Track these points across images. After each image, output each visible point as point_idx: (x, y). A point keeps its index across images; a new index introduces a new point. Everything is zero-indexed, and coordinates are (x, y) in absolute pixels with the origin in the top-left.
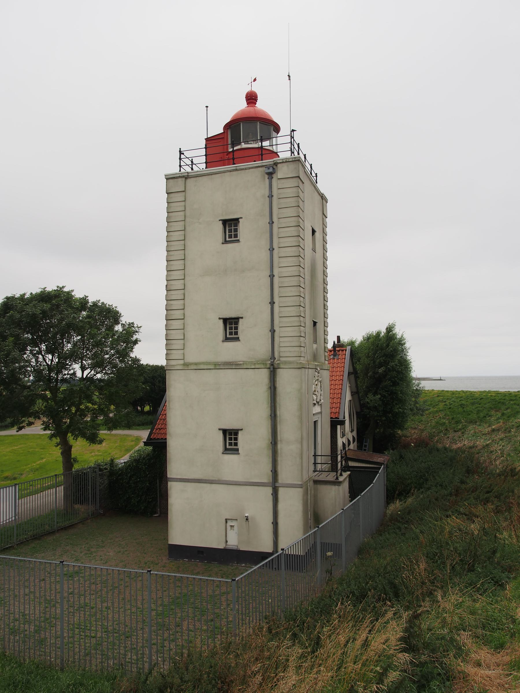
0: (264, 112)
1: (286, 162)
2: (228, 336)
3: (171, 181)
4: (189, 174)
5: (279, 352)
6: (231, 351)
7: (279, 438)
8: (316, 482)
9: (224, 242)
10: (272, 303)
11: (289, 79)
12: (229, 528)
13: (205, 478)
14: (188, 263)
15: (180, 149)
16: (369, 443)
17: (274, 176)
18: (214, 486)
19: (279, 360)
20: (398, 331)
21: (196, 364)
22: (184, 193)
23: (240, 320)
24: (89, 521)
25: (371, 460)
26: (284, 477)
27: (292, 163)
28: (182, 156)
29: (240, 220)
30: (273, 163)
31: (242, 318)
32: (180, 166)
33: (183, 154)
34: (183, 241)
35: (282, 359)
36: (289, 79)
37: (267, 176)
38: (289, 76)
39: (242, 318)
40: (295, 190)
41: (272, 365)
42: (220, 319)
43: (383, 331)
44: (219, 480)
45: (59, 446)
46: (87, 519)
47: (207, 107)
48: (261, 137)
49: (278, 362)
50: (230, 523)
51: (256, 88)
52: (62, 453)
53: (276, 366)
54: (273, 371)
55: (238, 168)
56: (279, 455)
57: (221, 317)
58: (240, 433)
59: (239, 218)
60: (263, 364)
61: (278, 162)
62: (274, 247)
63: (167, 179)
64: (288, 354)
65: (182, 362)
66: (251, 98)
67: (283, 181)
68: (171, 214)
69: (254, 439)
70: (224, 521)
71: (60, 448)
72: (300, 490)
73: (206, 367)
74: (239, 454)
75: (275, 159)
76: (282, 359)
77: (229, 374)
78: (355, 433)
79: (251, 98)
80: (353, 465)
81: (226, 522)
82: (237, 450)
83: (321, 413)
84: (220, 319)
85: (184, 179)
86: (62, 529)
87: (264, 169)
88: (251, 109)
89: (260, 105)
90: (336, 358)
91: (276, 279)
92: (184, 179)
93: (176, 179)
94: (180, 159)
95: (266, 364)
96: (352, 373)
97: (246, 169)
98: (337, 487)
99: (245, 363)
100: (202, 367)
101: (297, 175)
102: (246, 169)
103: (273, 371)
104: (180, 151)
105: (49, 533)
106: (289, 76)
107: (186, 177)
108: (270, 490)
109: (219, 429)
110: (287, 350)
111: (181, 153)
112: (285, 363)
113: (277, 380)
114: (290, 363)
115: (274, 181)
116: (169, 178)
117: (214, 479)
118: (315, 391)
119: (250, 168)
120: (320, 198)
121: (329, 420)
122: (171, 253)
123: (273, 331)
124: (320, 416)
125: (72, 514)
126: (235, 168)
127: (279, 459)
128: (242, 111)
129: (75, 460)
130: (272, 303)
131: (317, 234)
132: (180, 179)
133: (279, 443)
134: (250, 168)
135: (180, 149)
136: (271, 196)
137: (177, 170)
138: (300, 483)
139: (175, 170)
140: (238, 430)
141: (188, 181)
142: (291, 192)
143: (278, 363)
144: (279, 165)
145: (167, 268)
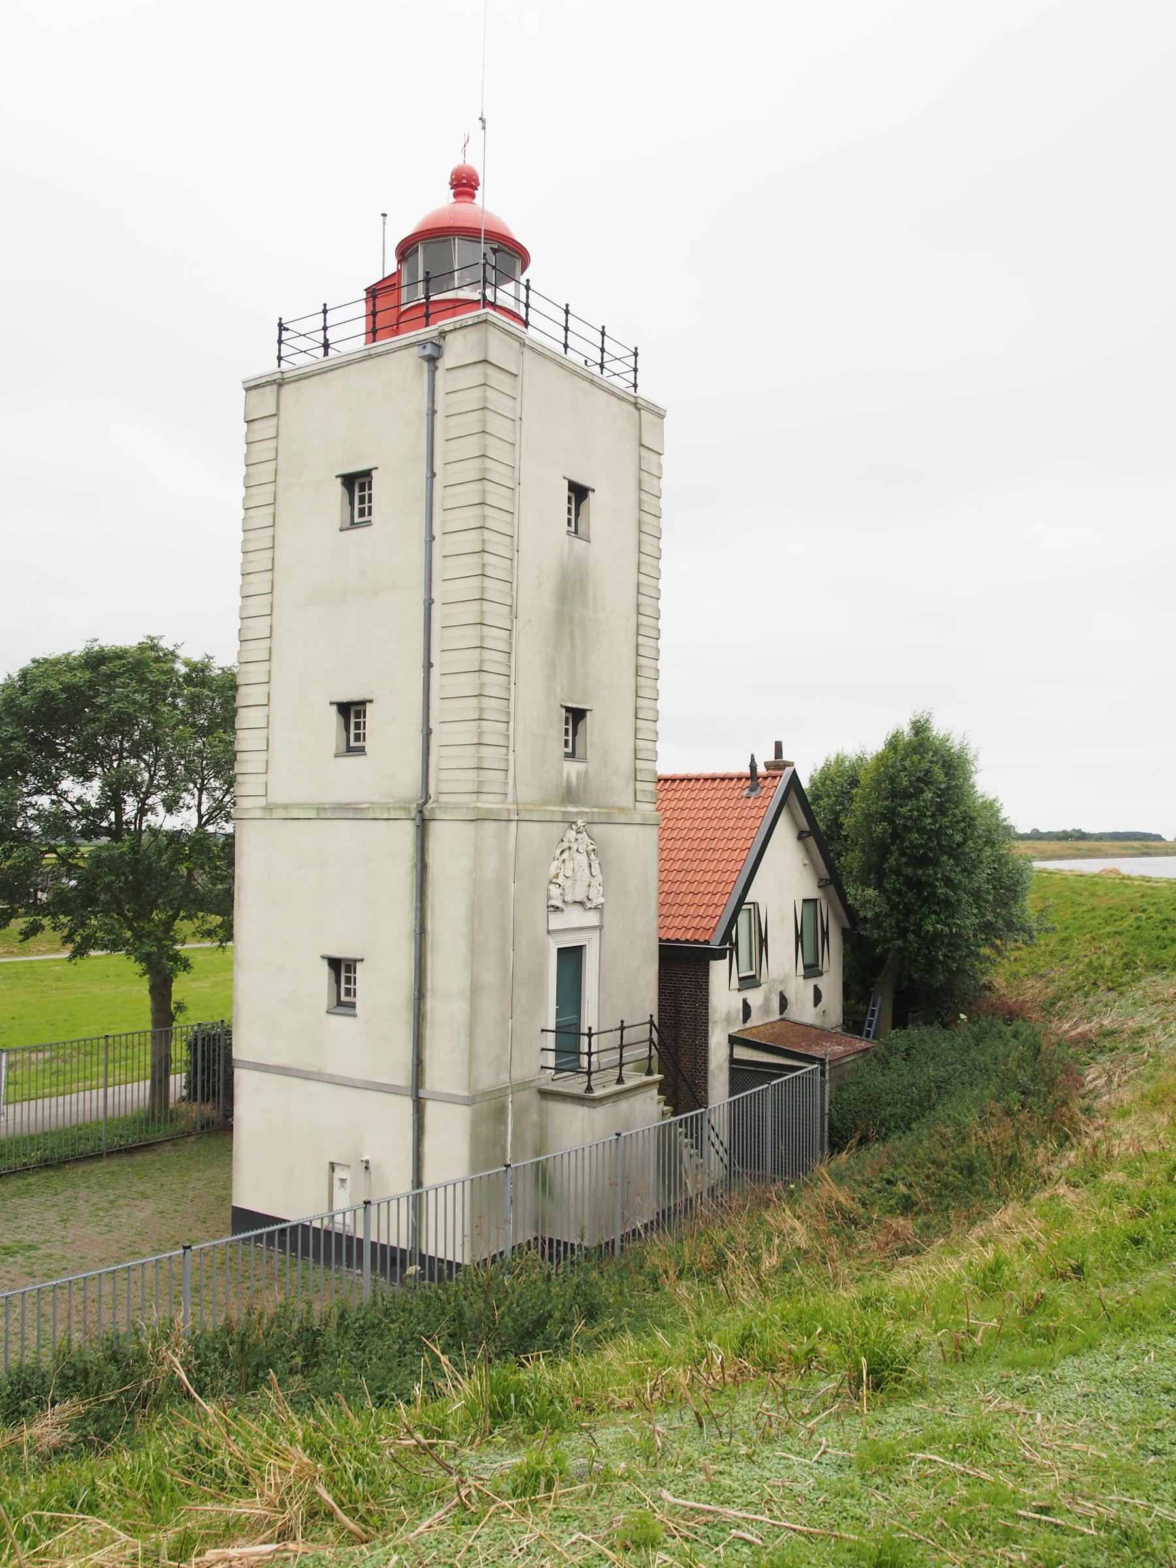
1: (461, 328)
2: (352, 744)
3: (253, 393)
4: (285, 376)
5: (438, 781)
6: (355, 779)
7: (429, 986)
8: (544, 1094)
9: (348, 525)
10: (428, 666)
11: (484, 128)
12: (337, 1183)
13: (299, 1067)
14: (279, 577)
16: (881, 1006)
17: (440, 363)
18: (312, 1085)
19: (436, 801)
20: (939, 728)
21: (286, 807)
22: (275, 419)
23: (368, 705)
24: (193, 1139)
25: (810, 1053)
26: (438, 1078)
27: (470, 329)
28: (285, 335)
29: (374, 473)
30: (436, 333)
32: (635, 370)
33: (287, 329)
34: (271, 529)
35: (443, 798)
37: (425, 364)
39: (371, 701)
40: (478, 392)
41: (421, 812)
42: (331, 703)
43: (907, 730)
44: (320, 1073)
45: (147, 976)
46: (189, 1134)
47: (384, 215)
48: (427, 273)
49: (434, 805)
50: (339, 1173)
51: (474, 162)
52: (152, 990)
53: (427, 815)
54: (423, 825)
55: (373, 352)
56: (428, 1025)
57: (334, 700)
58: (359, 966)
59: (371, 470)
60: (405, 809)
61: (447, 329)
62: (434, 533)
63: (247, 390)
64: (453, 787)
65: (262, 802)
66: (464, 184)
67: (455, 373)
68: (252, 468)
69: (383, 985)
70: (327, 1167)
71: (150, 980)
72: (465, 1110)
73: (301, 815)
74: (355, 1016)
75: (440, 323)
76: (443, 799)
77: (343, 832)
78: (831, 982)
79: (464, 184)
80: (760, 1059)
81: (333, 1170)
82: (353, 1005)
83: (600, 928)
84: (331, 703)
85: (275, 387)
86: (119, 1152)
87: (415, 350)
88: (464, 207)
90: (753, 794)
91: (436, 608)
92: (275, 387)
93: (261, 390)
94: (280, 342)
95: (409, 809)
96: (809, 834)
97: (387, 353)
98: (586, 1109)
99: (373, 805)
100: (296, 813)
101: (481, 358)
102: (387, 353)
103: (423, 825)
104: (280, 325)
105: (86, 1158)
107: (280, 383)
108: (407, 1104)
110: (452, 780)
111: (282, 327)
112: (447, 807)
113: (430, 848)
114: (455, 807)
115: (440, 374)
116: (252, 388)
117: (311, 1069)
118: (557, 876)
119: (395, 350)
120: (631, 409)
121: (657, 944)
122: (250, 556)
123: (427, 733)
124: (596, 935)
127: (428, 1033)
129: (180, 1007)
130: (428, 666)
132: (268, 389)
133: (429, 995)
134: (395, 350)
136: (433, 412)
137: (273, 366)
138: (466, 1094)
139: (269, 366)
140: (355, 961)
141: (286, 390)
142: (471, 399)
143: (432, 808)
144: (449, 337)
145: (241, 591)
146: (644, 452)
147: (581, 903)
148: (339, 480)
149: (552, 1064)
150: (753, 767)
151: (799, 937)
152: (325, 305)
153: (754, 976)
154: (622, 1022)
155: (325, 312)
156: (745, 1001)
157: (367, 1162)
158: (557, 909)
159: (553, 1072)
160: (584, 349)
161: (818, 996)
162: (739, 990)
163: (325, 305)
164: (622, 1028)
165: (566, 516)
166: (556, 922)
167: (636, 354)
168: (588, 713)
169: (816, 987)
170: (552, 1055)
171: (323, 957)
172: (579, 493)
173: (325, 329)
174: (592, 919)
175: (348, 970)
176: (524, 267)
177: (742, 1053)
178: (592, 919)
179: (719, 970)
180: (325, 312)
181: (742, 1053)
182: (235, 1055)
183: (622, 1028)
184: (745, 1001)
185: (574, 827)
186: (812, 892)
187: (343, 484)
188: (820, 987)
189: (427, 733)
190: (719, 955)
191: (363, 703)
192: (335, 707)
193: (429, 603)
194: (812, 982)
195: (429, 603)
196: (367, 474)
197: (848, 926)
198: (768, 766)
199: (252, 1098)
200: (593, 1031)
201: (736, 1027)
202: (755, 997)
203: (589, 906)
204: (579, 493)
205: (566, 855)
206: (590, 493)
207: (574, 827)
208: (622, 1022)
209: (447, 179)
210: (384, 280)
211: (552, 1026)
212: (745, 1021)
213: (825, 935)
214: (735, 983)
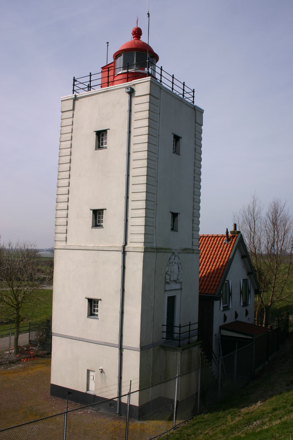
0: (126, 43)
11: (149, 16)
15: (74, 77)
23: (104, 211)
28: (76, 83)
29: (108, 131)
31: (106, 209)
32: (193, 97)
36: (149, 16)
38: (148, 14)
39: (106, 209)
42: (91, 210)
47: (108, 43)
54: (124, 253)
55: (108, 90)
59: (107, 130)
66: (138, 33)
79: (138, 33)
83: (181, 289)
89: (144, 39)
94: (74, 85)
103: (124, 253)
106: (148, 14)
109: (86, 298)
111: (75, 80)
120: (193, 110)
125: (111, 416)
126: (106, 90)
128: (131, 43)
131: (183, 142)
135: (74, 77)
146: (197, 125)
147: (175, 281)
148: (95, 133)
149: (165, 337)
150: (227, 232)
151: (241, 293)
152: (90, 73)
153: (227, 306)
154: (190, 322)
155: (90, 76)
156: (225, 315)
157: (101, 369)
158: (168, 283)
159: (165, 339)
160: (178, 90)
161: (247, 313)
162: (223, 311)
163: (90, 73)
164: (190, 325)
165: (173, 147)
166: (168, 288)
167: (194, 92)
168: (179, 215)
169: (246, 310)
170: (165, 333)
171: (86, 298)
172: (177, 138)
173: (90, 81)
174: (178, 286)
175: (95, 303)
176: (157, 61)
177: (225, 333)
178: (178, 286)
179: (216, 303)
180: (90, 76)
181: (225, 333)
182: (53, 331)
183: (190, 325)
184: (225, 315)
185: (174, 254)
186: (246, 277)
187: (97, 134)
188: (248, 310)
189: (127, 221)
190: (218, 299)
191: (102, 210)
192: (92, 211)
193: (128, 175)
194: (245, 308)
195: (128, 175)
196: (105, 131)
197: (257, 288)
198: (231, 232)
199: (58, 346)
200: (181, 326)
201: (222, 323)
202: (227, 313)
203: (178, 282)
204: (177, 138)
205: (171, 264)
206: (180, 139)
207: (174, 254)
208: (190, 322)
209: (131, 32)
210: (107, 65)
211: (165, 324)
212: (224, 322)
213: (249, 291)
214: (222, 309)
